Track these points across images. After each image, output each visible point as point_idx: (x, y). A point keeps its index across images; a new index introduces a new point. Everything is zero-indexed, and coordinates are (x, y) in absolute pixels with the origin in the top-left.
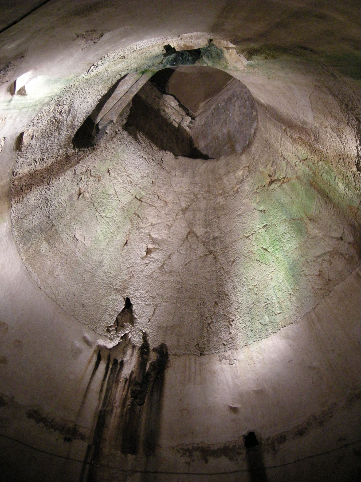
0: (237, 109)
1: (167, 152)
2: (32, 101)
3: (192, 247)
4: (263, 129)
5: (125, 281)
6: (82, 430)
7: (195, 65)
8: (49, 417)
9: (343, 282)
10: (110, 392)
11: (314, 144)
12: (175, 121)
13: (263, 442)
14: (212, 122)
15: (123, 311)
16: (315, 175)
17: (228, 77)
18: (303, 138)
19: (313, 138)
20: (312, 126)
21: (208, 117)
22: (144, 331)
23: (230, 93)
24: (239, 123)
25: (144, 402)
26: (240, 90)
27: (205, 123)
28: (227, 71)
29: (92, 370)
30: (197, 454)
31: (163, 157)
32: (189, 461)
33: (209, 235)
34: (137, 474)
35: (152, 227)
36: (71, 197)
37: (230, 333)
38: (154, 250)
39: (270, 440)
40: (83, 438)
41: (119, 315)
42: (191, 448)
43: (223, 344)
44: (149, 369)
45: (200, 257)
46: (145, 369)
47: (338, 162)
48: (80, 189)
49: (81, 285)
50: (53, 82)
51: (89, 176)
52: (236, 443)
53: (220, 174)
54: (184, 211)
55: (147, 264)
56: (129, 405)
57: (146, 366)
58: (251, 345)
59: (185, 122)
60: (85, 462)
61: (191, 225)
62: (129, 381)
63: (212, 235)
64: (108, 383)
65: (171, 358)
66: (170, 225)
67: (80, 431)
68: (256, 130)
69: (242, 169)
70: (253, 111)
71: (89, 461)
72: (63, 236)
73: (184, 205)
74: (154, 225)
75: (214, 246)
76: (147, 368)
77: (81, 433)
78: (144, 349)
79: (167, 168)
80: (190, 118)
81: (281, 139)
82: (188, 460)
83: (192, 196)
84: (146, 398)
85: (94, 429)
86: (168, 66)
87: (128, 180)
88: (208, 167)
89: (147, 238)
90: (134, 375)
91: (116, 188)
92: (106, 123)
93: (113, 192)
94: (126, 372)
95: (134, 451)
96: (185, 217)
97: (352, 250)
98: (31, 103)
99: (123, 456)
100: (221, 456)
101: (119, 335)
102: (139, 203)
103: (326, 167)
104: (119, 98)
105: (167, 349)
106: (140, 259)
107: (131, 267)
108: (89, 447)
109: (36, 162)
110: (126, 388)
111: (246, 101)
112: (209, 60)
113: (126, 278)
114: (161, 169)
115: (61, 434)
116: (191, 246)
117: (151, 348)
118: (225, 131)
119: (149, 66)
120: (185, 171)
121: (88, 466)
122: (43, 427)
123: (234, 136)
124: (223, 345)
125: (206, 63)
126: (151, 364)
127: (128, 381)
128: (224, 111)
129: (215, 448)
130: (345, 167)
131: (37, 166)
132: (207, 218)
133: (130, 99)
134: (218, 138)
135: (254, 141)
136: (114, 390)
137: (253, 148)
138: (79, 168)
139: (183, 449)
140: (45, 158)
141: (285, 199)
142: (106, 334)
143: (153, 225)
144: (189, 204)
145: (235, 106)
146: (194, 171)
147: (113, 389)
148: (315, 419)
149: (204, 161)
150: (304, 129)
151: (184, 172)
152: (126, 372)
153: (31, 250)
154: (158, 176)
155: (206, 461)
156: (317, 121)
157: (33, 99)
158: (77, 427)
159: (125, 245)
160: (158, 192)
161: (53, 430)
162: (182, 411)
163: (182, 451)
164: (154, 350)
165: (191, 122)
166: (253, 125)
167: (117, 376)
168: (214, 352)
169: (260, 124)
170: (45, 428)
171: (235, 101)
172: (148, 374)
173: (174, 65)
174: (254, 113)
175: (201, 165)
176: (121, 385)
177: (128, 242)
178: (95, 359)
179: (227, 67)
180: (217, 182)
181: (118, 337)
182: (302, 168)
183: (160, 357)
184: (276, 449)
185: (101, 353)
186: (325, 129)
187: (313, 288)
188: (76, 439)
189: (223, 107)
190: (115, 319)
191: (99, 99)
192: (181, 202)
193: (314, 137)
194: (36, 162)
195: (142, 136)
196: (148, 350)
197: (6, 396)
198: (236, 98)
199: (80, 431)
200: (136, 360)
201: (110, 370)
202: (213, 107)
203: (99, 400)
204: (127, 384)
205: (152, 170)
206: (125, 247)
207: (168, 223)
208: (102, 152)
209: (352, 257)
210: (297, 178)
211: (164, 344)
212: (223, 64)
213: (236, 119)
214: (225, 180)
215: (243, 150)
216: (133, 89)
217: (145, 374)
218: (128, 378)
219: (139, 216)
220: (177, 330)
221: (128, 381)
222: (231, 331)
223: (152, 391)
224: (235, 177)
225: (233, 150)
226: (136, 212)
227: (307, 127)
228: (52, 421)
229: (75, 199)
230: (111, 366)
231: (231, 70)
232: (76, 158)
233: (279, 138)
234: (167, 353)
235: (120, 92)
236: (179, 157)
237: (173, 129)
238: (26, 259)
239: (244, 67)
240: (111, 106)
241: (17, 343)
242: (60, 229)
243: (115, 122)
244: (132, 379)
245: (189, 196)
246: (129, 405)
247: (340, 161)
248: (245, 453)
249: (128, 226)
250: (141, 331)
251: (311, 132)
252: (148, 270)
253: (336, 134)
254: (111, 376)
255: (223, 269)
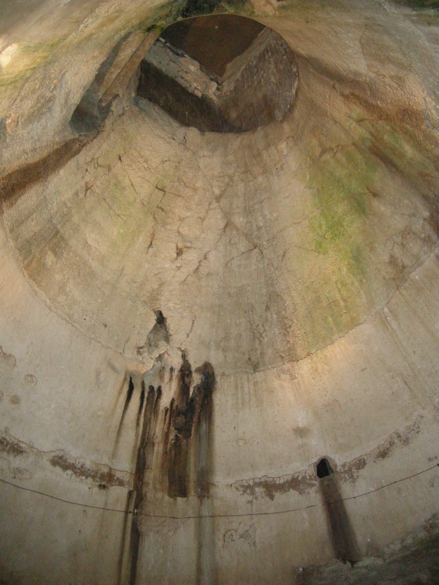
0: (272, 66)
1: (190, 128)
2: (10, 76)
3: (232, 241)
4: (306, 87)
5: (153, 290)
6: (118, 475)
7: (213, 14)
8: (77, 463)
9: (420, 268)
10: (148, 427)
11: (371, 100)
12: (198, 89)
13: (338, 470)
14: (244, 86)
15: (155, 327)
16: (376, 139)
17: (259, 27)
18: (357, 93)
19: (369, 93)
20: (366, 77)
21: (238, 80)
22: (182, 349)
23: (262, 48)
24: (276, 85)
25: (191, 435)
26: (274, 42)
27: (235, 88)
28: (255, 19)
29: (125, 402)
30: (259, 490)
31: (186, 134)
32: (251, 499)
33: (251, 225)
34: (191, 519)
35: (180, 222)
36: (77, 194)
37: (288, 342)
38: (185, 250)
39: (347, 466)
40: (121, 483)
41: (150, 332)
42: (252, 483)
43: (281, 356)
44: (193, 394)
45: (243, 253)
46: (189, 394)
47: (402, 120)
48: (86, 183)
49: (100, 301)
50: (34, 50)
51: (96, 166)
52: (305, 473)
53: (258, 149)
54: (218, 199)
55: (179, 268)
56: (172, 440)
57: (189, 390)
58: (315, 354)
59: (210, 90)
60: (127, 512)
61: (228, 216)
62: (172, 411)
63: (254, 226)
64: (145, 415)
65: (218, 379)
66: (203, 217)
67: (117, 476)
68: (298, 89)
69: (285, 140)
70: (293, 66)
71: (131, 509)
72: (73, 242)
73: (217, 191)
74: (183, 219)
75: (259, 238)
76: (191, 393)
77: (118, 479)
78: (185, 372)
79: (192, 148)
80: (216, 84)
81: (330, 97)
82: (250, 498)
83: (227, 180)
84: (193, 429)
85: (134, 472)
86: (180, 19)
87: (146, 167)
88: (243, 142)
89: (176, 236)
90: (176, 403)
91: (131, 179)
92: (111, 98)
93: (129, 184)
94: (165, 401)
95: (184, 493)
96: (219, 206)
97: (428, 227)
98: (9, 79)
99: (171, 500)
100: (289, 491)
101: (153, 357)
102: (161, 193)
103: (388, 128)
104: (123, 65)
105: (212, 368)
106: (169, 262)
107: (159, 273)
108: (130, 494)
109: (27, 153)
110: (167, 419)
111: (283, 56)
112: (230, 6)
113: (155, 286)
114: (184, 150)
115: (94, 481)
116: (230, 241)
117: (193, 368)
118: (260, 96)
119: (156, 20)
120: (215, 150)
121: (130, 516)
122: (72, 475)
123: (272, 101)
124: (280, 357)
125: (226, 10)
126: (195, 387)
127: (169, 411)
128: (258, 71)
129: (282, 481)
130: (412, 126)
131: (29, 159)
132: (247, 205)
133: (137, 65)
134: (252, 105)
135: (297, 104)
136: (153, 423)
137: (296, 113)
138: (82, 157)
139: (242, 486)
140: (38, 148)
141: (340, 172)
142: (137, 357)
143: (182, 220)
144: (223, 189)
145: (270, 63)
146: (226, 149)
147: (152, 422)
148: (399, 436)
149: (237, 135)
150: (358, 82)
151: (214, 150)
152: (165, 401)
153: (34, 264)
154: (182, 159)
155: (272, 497)
156: (372, 70)
157: (11, 74)
158: (113, 471)
159: (149, 247)
160: (184, 178)
161: (84, 477)
162: (237, 441)
163: (242, 489)
164: (198, 370)
165: (218, 89)
166: (294, 85)
167: (156, 406)
168: (270, 367)
169: (302, 81)
170: (74, 476)
171: (270, 57)
172: (192, 400)
173: (187, 16)
174: (295, 70)
175: (235, 141)
176: (161, 416)
177: (153, 243)
178: (126, 388)
179: (254, 12)
180: (256, 159)
181: (152, 359)
182: (359, 132)
183: (205, 378)
184: (355, 477)
185: (133, 381)
186: (383, 80)
187: (384, 278)
188: (113, 485)
189: (256, 66)
190: (145, 338)
191: (97, 68)
192: (214, 188)
193: (371, 90)
194: (27, 153)
195: (157, 111)
196: (191, 372)
197: (23, 442)
198: (270, 53)
199: (117, 476)
200: (176, 386)
201: (145, 399)
202: (243, 67)
203: (137, 437)
204: (168, 415)
205: (174, 152)
206: (150, 249)
207: (200, 215)
208: (109, 135)
209: (429, 236)
210: (354, 144)
211: (209, 363)
212: (249, 10)
213: (273, 79)
214: (265, 155)
215: (284, 116)
216: (139, 53)
217: (189, 401)
218: (169, 407)
219: (163, 210)
220: (222, 344)
221: (169, 411)
222: (288, 339)
223: (199, 422)
224: (277, 150)
225: (271, 118)
226: (159, 206)
227: (361, 80)
228: (82, 467)
229: (81, 195)
230: (146, 395)
231: (258, 16)
232: (77, 145)
233: (328, 97)
234: (213, 373)
235: (123, 57)
236: (207, 133)
237: (196, 99)
238: (28, 274)
239: (276, 11)
240: (114, 76)
241: (29, 378)
242: (67, 235)
243: (121, 96)
244: (174, 408)
245: (222, 179)
246: (172, 440)
247: (405, 118)
248: (318, 484)
249: (150, 223)
250: (179, 349)
251: (366, 85)
252: (181, 275)
253: (397, 84)
254: (148, 406)
255: (272, 264)
